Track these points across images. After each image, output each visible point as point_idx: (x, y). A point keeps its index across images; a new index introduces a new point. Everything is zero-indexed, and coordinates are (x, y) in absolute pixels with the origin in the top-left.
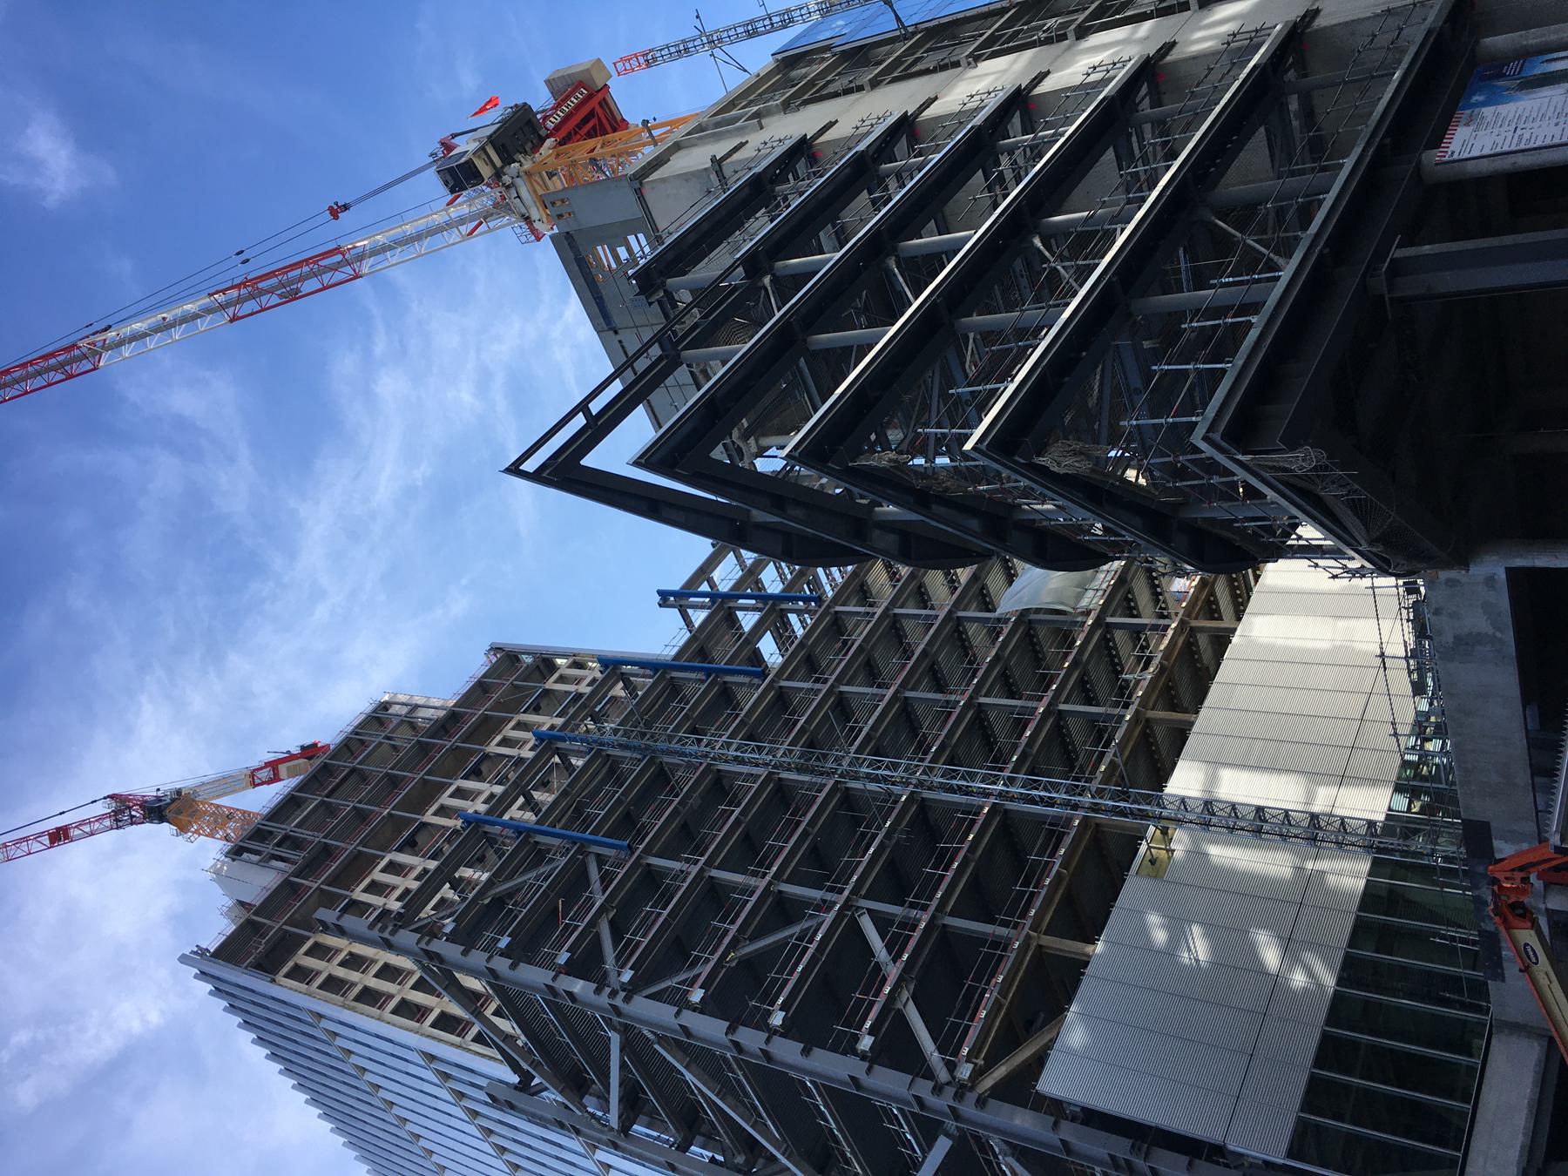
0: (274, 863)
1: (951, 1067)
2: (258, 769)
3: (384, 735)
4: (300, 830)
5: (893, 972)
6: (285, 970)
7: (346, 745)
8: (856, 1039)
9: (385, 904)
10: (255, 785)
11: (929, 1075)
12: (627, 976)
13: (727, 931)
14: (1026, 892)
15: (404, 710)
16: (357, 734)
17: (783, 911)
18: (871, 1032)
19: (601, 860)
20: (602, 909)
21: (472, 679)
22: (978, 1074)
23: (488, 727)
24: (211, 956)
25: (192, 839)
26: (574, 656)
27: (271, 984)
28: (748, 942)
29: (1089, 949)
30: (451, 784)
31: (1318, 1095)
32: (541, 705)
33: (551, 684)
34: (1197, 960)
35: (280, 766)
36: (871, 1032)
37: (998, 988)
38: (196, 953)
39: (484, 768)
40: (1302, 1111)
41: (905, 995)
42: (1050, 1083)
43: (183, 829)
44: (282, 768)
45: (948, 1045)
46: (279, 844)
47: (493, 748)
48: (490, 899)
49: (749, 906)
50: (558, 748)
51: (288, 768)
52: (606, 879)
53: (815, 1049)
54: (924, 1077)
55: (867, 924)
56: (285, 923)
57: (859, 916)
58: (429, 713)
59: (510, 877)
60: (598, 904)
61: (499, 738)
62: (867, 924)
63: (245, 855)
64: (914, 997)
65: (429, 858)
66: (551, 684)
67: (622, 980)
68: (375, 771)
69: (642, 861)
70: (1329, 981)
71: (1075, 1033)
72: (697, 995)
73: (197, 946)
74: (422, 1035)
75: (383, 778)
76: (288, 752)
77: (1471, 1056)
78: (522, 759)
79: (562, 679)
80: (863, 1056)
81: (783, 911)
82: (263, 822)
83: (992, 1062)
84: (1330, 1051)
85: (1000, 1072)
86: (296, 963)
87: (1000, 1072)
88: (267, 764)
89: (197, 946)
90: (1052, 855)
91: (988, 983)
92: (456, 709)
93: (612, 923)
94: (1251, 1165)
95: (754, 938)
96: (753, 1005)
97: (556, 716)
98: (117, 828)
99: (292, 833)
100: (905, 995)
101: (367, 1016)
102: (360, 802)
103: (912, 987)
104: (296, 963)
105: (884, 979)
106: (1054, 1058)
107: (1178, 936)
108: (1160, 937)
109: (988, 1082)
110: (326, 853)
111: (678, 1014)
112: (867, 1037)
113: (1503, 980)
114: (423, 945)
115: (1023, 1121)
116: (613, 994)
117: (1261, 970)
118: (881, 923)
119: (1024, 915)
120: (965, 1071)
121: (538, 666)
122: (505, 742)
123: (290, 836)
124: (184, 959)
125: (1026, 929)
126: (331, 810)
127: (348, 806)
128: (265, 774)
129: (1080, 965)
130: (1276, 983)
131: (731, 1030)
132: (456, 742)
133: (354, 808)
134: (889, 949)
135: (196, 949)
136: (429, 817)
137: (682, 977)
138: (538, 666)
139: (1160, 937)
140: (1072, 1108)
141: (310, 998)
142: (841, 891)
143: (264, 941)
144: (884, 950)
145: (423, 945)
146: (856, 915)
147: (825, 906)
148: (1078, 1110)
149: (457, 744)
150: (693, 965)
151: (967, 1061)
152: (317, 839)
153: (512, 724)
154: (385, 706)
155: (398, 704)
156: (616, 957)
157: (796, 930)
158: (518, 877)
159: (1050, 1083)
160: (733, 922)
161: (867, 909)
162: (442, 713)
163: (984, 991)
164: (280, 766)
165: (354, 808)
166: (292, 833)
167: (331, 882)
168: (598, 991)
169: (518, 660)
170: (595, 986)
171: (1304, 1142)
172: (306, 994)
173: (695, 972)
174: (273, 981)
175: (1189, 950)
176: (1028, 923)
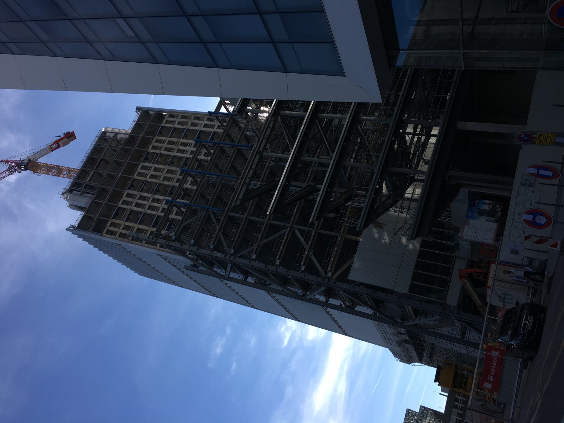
0: (85, 194)
1: (326, 273)
2: (52, 145)
3: (108, 145)
4: (90, 183)
5: (307, 247)
6: (105, 232)
7: (95, 149)
8: (300, 267)
9: (131, 208)
10: (53, 150)
11: (320, 276)
12: (232, 251)
13: (258, 237)
14: (340, 222)
15: (112, 135)
16: (98, 145)
17: (273, 229)
18: (304, 265)
19: (215, 215)
20: (219, 230)
21: (134, 122)
22: (333, 274)
23: (146, 142)
24: (77, 228)
25: (40, 175)
26: (169, 112)
27: (101, 236)
28: (264, 239)
29: (358, 238)
30: (140, 164)
31: (415, 277)
32: (162, 132)
33: (163, 124)
34: (386, 242)
35: (59, 142)
36: (304, 265)
37: (335, 251)
38: (71, 227)
39: (148, 157)
40: (412, 281)
41: (311, 253)
42: (351, 277)
43: (35, 172)
44: (60, 143)
45: (325, 268)
46: (85, 188)
47: (150, 150)
48: (182, 227)
49: (263, 229)
50: (189, 173)
51: (63, 143)
52: (218, 220)
53: (290, 270)
54: (319, 276)
55: (297, 232)
56: (98, 216)
57: (295, 230)
58: (122, 136)
59: (186, 221)
60: (218, 229)
61: (121, 201)
62: (297, 232)
63: (74, 192)
64: (313, 254)
65: (140, 192)
66: (163, 124)
67: (231, 253)
68: (110, 159)
69: (227, 214)
70: (418, 246)
71: (357, 263)
72: (254, 257)
73: (70, 225)
74: (157, 250)
75: (114, 162)
76: (60, 136)
77: (450, 265)
78: (162, 154)
79: (167, 122)
80: (302, 271)
81: (273, 229)
82: (76, 180)
83: (336, 271)
84: (418, 265)
85: (338, 273)
86: (107, 229)
87: (338, 273)
88: (55, 142)
89: (70, 225)
90: (346, 211)
91: (333, 250)
92: (131, 134)
93: (223, 234)
94: (400, 294)
95: (266, 238)
96: (270, 259)
97: (169, 137)
98: (11, 174)
99: (88, 184)
100: (311, 253)
101: (138, 245)
102: (108, 172)
103: (312, 251)
104: (107, 229)
105: (305, 250)
106: (352, 270)
107: (381, 236)
108: (376, 235)
109: (335, 276)
110: (103, 191)
111: (250, 262)
112: (303, 266)
113: (459, 250)
114: (167, 243)
115: (345, 286)
116: (230, 257)
117: (402, 244)
118: (302, 232)
119: (340, 229)
120: (330, 274)
121: (157, 116)
122: (154, 147)
123: (88, 185)
124: (67, 229)
125: (341, 234)
126: (100, 175)
127: (105, 173)
128: (54, 146)
129: (357, 242)
130: (406, 247)
131: (266, 266)
132: (136, 148)
133: (107, 174)
134: (305, 240)
135: (70, 226)
136: (135, 177)
137: (248, 250)
138: (157, 116)
139: (376, 235)
140: (357, 282)
141: (116, 240)
142: (289, 223)
143: (94, 222)
144: (304, 241)
145: (167, 243)
146: (294, 230)
147: (284, 228)
148: (358, 283)
149: (136, 149)
150: (251, 245)
151: (330, 272)
152: (98, 186)
153: (154, 141)
154: (104, 133)
155: (109, 132)
156: (227, 246)
157: (278, 235)
158: (189, 219)
159: (351, 277)
160: (259, 234)
161: (297, 228)
162: (127, 136)
163: (332, 252)
164: (59, 142)
165: (107, 174)
166: (88, 184)
167: (109, 200)
168: (225, 256)
169: (149, 113)
170: (224, 255)
171: (413, 288)
172: (114, 239)
173: (251, 249)
174: (102, 235)
175: (384, 239)
176: (342, 232)
